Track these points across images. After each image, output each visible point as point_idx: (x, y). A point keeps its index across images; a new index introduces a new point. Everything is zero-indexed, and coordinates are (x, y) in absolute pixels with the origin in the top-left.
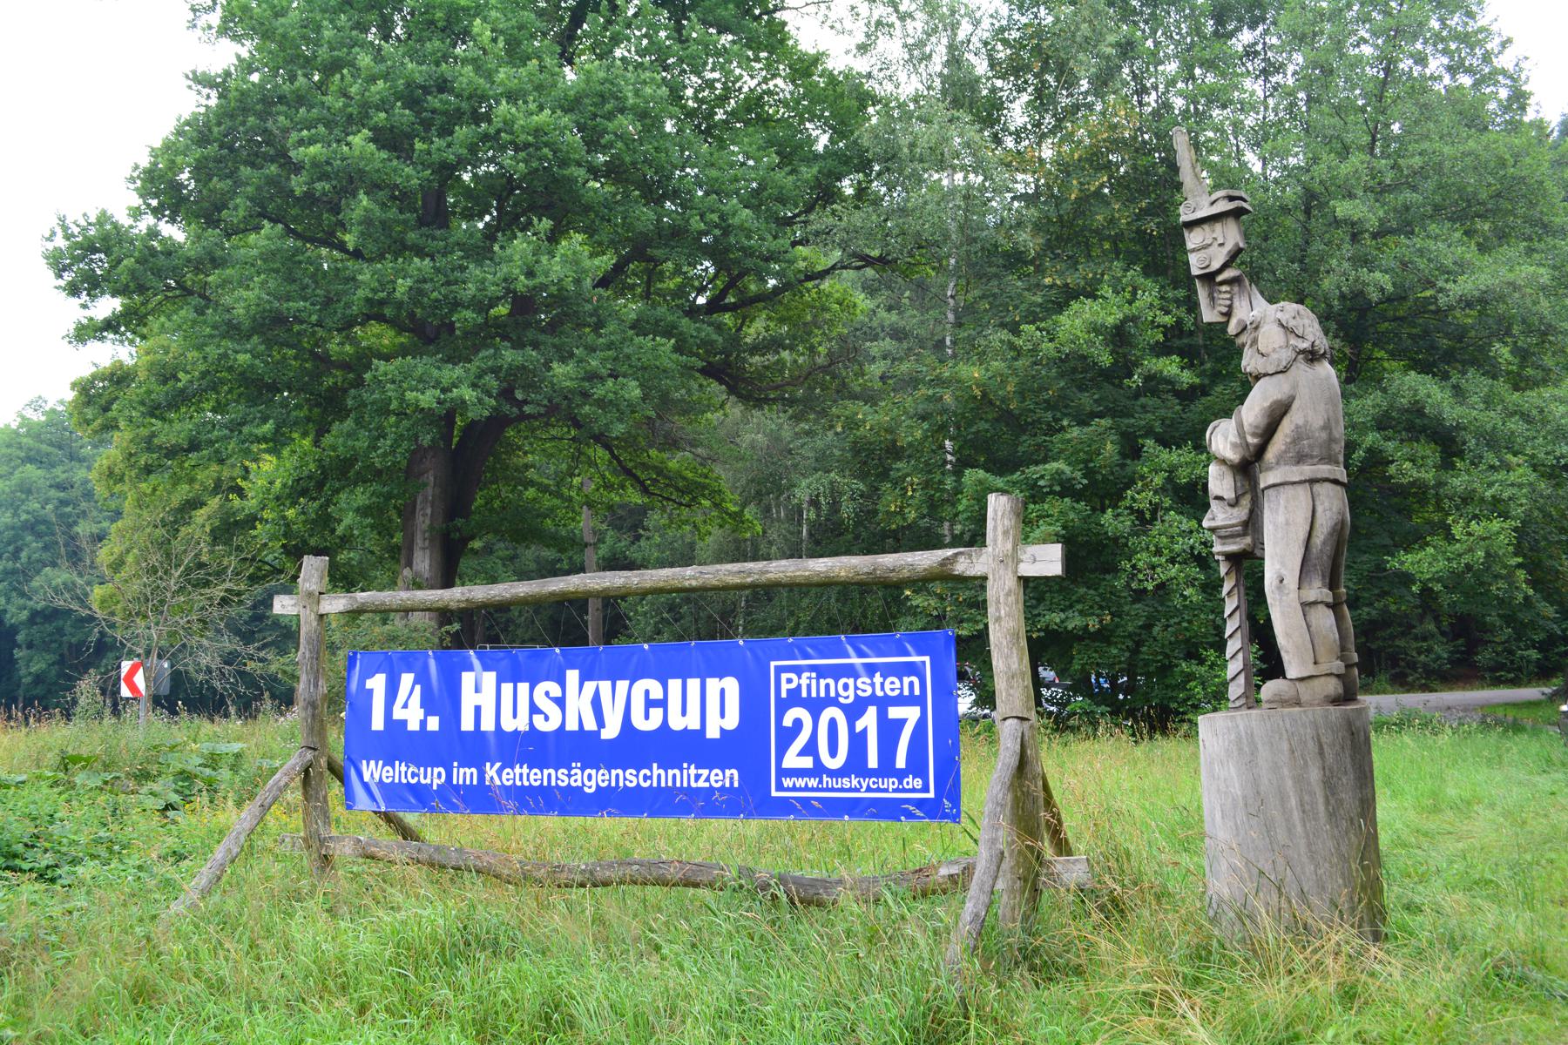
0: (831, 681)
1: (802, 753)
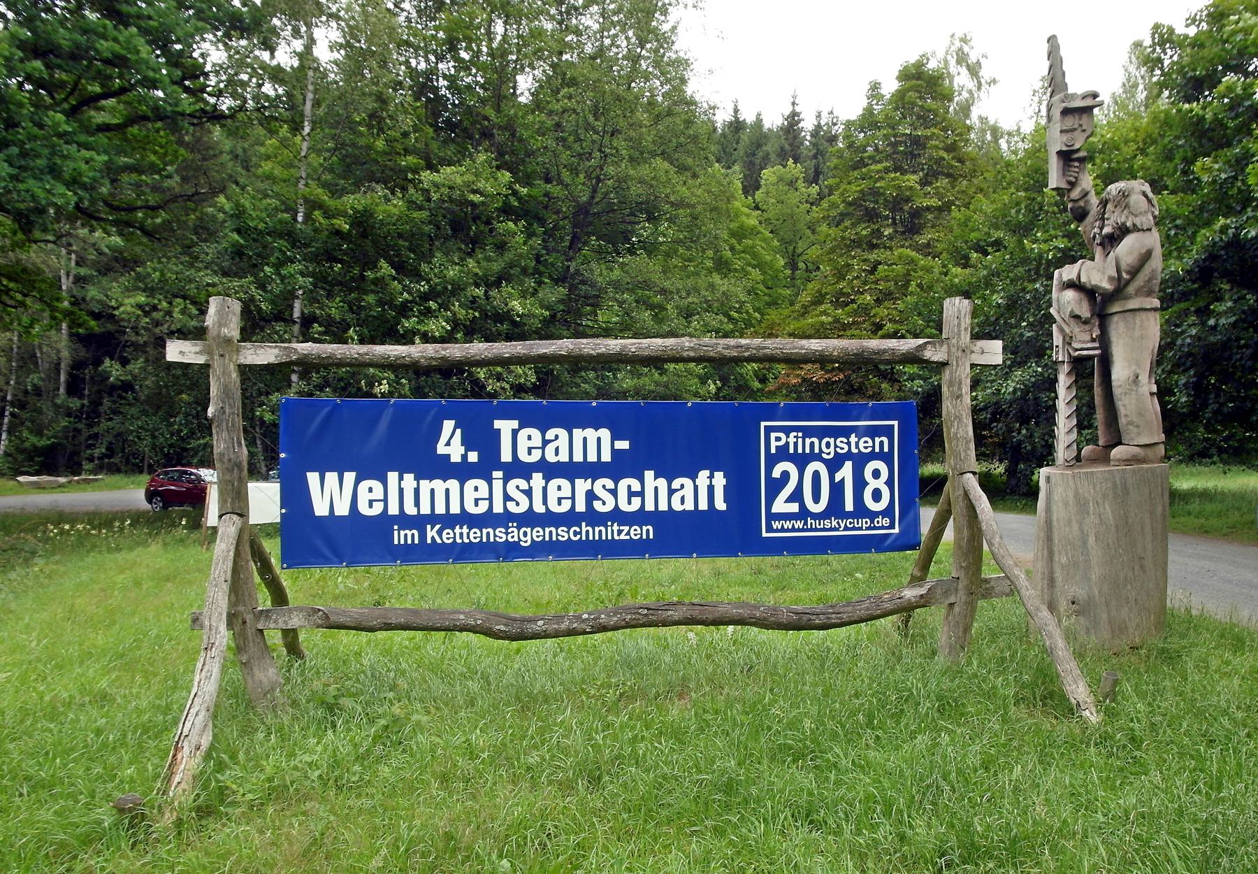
0: (815, 440)
1: (789, 500)
